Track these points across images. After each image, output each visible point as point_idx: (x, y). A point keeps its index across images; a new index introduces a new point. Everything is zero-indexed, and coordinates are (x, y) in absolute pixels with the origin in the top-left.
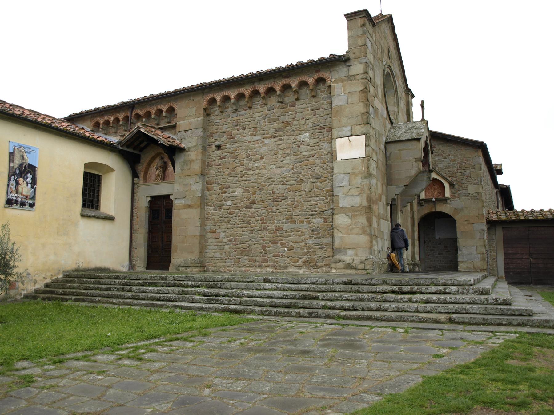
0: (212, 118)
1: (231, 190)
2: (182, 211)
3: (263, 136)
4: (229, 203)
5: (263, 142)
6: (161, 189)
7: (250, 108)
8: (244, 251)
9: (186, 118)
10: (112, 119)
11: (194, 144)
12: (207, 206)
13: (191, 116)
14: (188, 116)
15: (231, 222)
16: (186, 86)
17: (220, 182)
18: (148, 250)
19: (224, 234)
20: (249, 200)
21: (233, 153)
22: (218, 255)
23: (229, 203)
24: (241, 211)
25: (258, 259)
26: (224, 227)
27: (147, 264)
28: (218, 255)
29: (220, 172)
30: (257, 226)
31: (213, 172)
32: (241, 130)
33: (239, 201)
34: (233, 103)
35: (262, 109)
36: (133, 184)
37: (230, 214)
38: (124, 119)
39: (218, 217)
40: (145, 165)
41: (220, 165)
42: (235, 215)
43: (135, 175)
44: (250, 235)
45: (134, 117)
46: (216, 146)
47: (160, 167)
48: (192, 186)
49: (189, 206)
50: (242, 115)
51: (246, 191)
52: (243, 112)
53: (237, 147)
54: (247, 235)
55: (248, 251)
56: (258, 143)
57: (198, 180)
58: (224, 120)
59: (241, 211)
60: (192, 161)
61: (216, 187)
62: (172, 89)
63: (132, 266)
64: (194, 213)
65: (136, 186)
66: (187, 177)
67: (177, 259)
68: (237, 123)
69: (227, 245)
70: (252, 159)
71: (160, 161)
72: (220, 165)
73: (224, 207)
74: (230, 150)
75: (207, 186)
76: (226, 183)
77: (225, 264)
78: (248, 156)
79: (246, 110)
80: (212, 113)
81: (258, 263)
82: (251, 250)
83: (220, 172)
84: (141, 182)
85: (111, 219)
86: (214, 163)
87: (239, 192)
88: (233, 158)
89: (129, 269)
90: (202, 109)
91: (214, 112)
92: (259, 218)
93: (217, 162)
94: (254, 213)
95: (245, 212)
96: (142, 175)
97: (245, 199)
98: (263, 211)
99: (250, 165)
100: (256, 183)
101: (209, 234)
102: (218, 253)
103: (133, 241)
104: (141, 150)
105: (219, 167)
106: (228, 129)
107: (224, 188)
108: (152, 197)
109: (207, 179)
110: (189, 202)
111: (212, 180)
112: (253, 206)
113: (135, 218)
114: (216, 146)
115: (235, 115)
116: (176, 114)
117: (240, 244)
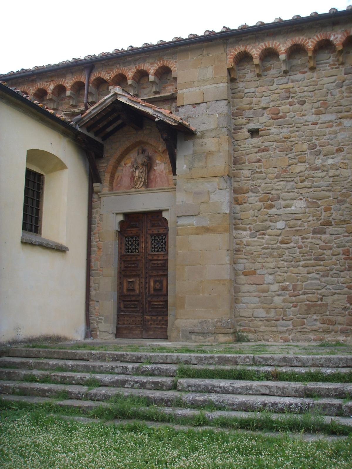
0: (240, 85)
1: (283, 203)
2: (192, 237)
3: (340, 115)
4: (280, 225)
5: (340, 124)
6: (144, 202)
7: (313, 69)
8: (313, 306)
9: (196, 84)
10: (52, 87)
11: (212, 126)
12: (236, 229)
13: (205, 80)
14: (198, 81)
15: (284, 257)
16: (52, 63)
17: (259, 189)
18: (119, 303)
19: (271, 277)
20: (318, 220)
21: (284, 142)
22: (261, 313)
23: (280, 225)
24: (302, 238)
25: (340, 319)
26: (272, 265)
27: (118, 329)
28: (261, 313)
29: (261, 172)
30: (336, 264)
31: (246, 173)
32: (297, 106)
33: (299, 222)
34: (284, 61)
35: (334, 72)
36: (91, 192)
37: (282, 242)
38: (73, 87)
39: (259, 248)
40: (112, 161)
41: (259, 161)
42: (292, 244)
43: (94, 177)
44: (323, 279)
45: (93, 83)
46: (250, 131)
47: (143, 164)
48: (212, 196)
49: (207, 230)
50: (297, 81)
51: (314, 203)
52: (299, 76)
53: (291, 132)
54: (316, 279)
55: (320, 305)
56: (331, 126)
57: (223, 185)
58: (264, 89)
59: (302, 238)
60: (211, 153)
61: (252, 198)
62: (110, 49)
63: (90, 332)
64: (219, 241)
65: (95, 196)
66: (201, 180)
67: (181, 319)
68: (289, 94)
69: (279, 295)
70: (320, 151)
71: (141, 156)
72: (259, 161)
73: (269, 231)
74: (277, 138)
75: (238, 195)
76: (273, 192)
77: (275, 329)
78: (312, 147)
79: (304, 73)
80: (240, 77)
81: (340, 327)
82: (327, 305)
83: (261, 172)
84: (106, 190)
85: (61, 249)
86: (246, 158)
87: (299, 205)
88: (284, 150)
89: (87, 336)
90: (226, 70)
91: (244, 76)
92: (340, 250)
93: (254, 157)
94: (330, 241)
95: (313, 241)
96: (106, 177)
97: (311, 218)
98: (347, 238)
99: (319, 162)
100: (330, 191)
101: (242, 277)
102: (261, 310)
103: (92, 289)
104: (104, 138)
105: (257, 164)
106: (272, 104)
107: (269, 200)
108: (126, 215)
109: (235, 185)
110: (207, 223)
111: (245, 185)
112: (328, 231)
113: (94, 249)
114: (250, 131)
115: (285, 80)
116: (176, 79)
117: (304, 294)
